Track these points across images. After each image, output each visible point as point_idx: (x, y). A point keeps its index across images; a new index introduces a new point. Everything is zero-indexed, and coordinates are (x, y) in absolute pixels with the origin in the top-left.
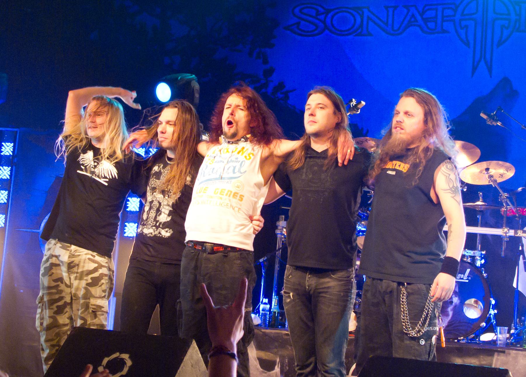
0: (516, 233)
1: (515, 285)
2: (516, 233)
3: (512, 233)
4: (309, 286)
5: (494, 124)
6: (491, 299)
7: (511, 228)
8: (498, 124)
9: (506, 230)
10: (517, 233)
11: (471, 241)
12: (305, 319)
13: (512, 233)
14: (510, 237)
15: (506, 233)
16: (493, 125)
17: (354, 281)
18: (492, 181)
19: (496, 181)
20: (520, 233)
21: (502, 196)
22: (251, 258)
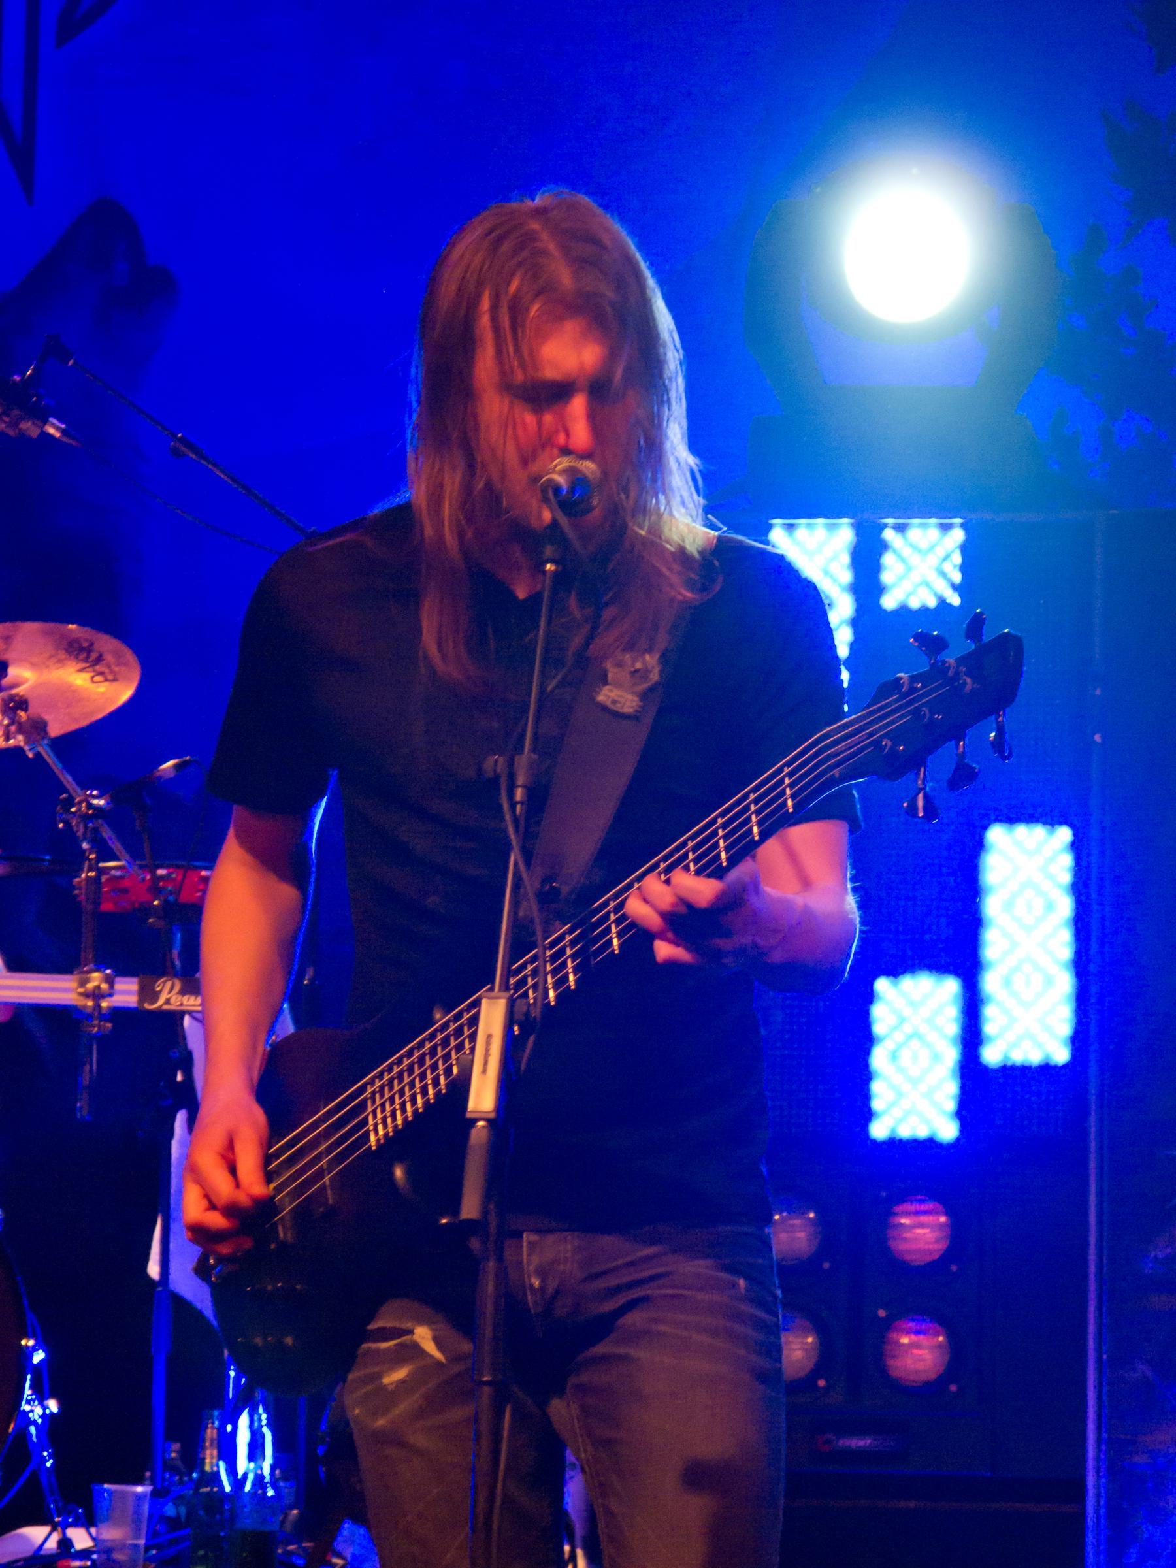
0: (148, 993)
1: (154, 1270)
2: (148, 993)
3: (126, 993)
4: (542, 1273)
5: (29, 428)
6: (23, 1342)
7: (124, 970)
8: (51, 431)
9: (96, 979)
10: (155, 996)
11: (165, 941)
12: (14, 691)
13: (126, 993)
14: (118, 1013)
15: (97, 995)
16: (23, 436)
17: (465, 304)
18: (20, 730)
19: (37, 728)
20: (169, 995)
21: (70, 802)
22: (142, 1550)
